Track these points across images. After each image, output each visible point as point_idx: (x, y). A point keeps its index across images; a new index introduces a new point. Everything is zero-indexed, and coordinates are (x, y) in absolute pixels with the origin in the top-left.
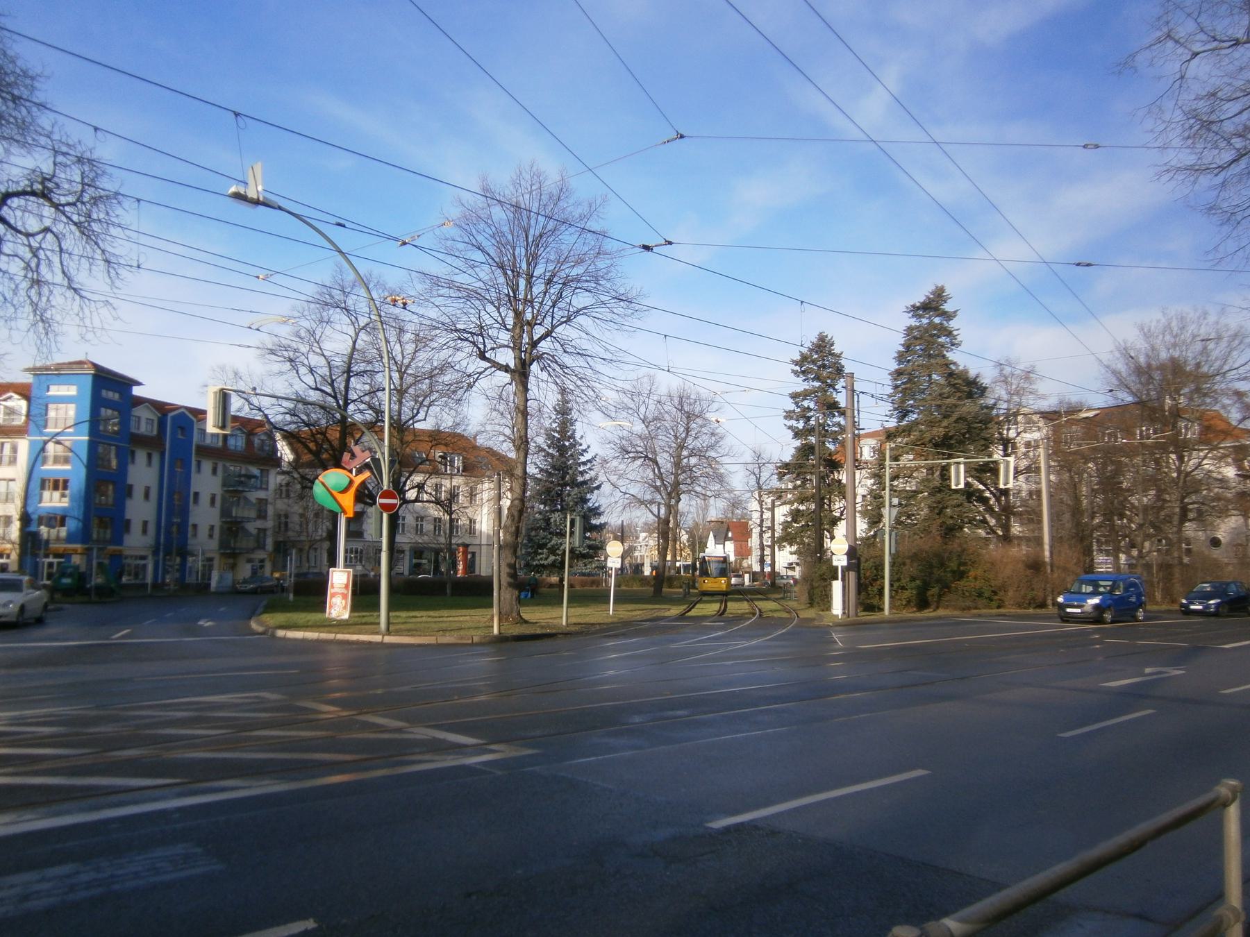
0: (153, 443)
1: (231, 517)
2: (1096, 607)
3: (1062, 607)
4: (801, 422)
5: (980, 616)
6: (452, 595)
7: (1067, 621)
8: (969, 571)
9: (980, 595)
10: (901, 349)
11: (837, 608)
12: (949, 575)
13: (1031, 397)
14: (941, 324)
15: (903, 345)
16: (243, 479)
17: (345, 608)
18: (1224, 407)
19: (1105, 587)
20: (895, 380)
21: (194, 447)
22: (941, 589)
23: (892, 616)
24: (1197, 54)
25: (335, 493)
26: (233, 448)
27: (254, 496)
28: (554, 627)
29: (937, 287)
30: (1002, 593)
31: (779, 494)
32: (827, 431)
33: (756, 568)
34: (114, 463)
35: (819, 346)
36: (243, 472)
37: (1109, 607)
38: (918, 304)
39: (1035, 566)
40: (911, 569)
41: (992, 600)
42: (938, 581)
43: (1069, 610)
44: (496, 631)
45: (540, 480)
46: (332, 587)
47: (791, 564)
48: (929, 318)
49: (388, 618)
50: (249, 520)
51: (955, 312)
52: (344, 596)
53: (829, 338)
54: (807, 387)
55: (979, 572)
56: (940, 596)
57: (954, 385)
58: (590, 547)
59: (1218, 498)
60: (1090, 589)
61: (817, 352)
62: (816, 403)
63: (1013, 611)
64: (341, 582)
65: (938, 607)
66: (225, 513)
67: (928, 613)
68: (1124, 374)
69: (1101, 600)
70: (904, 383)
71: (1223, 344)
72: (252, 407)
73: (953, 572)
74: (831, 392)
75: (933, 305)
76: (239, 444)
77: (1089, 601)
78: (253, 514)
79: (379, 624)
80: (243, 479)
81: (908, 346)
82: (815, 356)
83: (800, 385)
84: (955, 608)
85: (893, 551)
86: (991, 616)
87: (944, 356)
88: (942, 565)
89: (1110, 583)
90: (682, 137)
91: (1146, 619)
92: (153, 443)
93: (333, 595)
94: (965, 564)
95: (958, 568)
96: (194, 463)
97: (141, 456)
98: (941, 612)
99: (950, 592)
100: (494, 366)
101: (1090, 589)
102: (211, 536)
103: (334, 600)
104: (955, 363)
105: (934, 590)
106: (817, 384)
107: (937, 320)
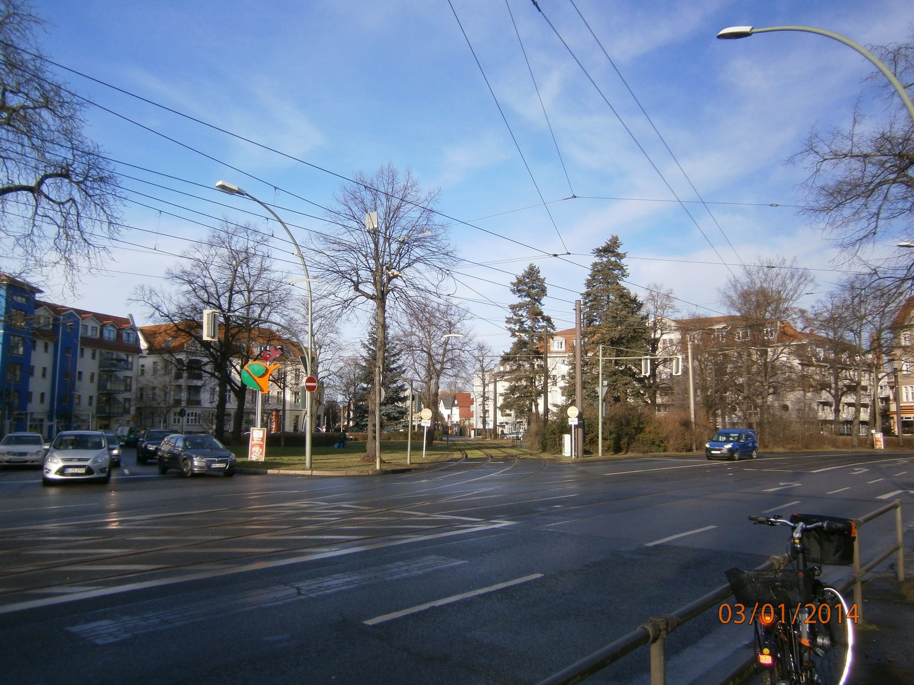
0: (50, 334)
1: (106, 389)
2: (729, 450)
3: (708, 450)
4: (517, 325)
5: (655, 456)
6: (285, 446)
7: (711, 459)
8: (645, 428)
9: (653, 443)
10: (589, 278)
11: (567, 451)
12: (633, 430)
13: (670, 310)
14: (616, 262)
15: (590, 275)
16: (114, 362)
17: (261, 454)
18: (793, 319)
19: (733, 437)
20: (585, 299)
21: (79, 338)
22: (629, 440)
23: (603, 457)
24: (826, 159)
25: (256, 377)
26: (107, 339)
27: (122, 374)
28: (404, 465)
29: (613, 237)
30: (666, 442)
31: (501, 375)
32: (534, 332)
33: (480, 426)
34: (21, 350)
35: (530, 273)
36: (114, 357)
37: (737, 450)
38: (601, 248)
39: (686, 424)
40: (612, 427)
41: (660, 447)
42: (627, 434)
43: (713, 452)
44: (378, 467)
45: (365, 367)
46: (253, 440)
47: (502, 423)
48: (608, 257)
49: (311, 459)
50: (119, 392)
51: (625, 254)
52: (261, 446)
53: (537, 268)
54: (521, 302)
55: (652, 428)
56: (628, 444)
57: (624, 303)
58: (399, 412)
59: (789, 379)
60: (724, 439)
61: (528, 278)
62: (528, 312)
63: (674, 453)
64: (259, 437)
65: (627, 452)
66: (101, 386)
67: (621, 455)
68: (734, 298)
69: (732, 446)
70: (591, 301)
71: (795, 280)
72: (162, 314)
73: (635, 428)
74: (538, 305)
75: (610, 249)
76: (112, 336)
77: (725, 446)
78: (122, 388)
79: (305, 464)
80: (114, 362)
81: (593, 277)
82: (527, 280)
83: (516, 300)
84: (639, 452)
85: (604, 415)
86: (661, 457)
87: (617, 284)
88: (628, 424)
89: (737, 435)
90: (575, 197)
91: (757, 457)
92: (50, 334)
93: (253, 446)
94: (642, 423)
95: (639, 426)
96: (79, 350)
97: (40, 345)
98: (629, 454)
99: (634, 441)
100: (363, 295)
101: (724, 439)
102: (90, 404)
103: (254, 449)
104: (625, 289)
105: (625, 440)
106: (528, 299)
107: (613, 259)
